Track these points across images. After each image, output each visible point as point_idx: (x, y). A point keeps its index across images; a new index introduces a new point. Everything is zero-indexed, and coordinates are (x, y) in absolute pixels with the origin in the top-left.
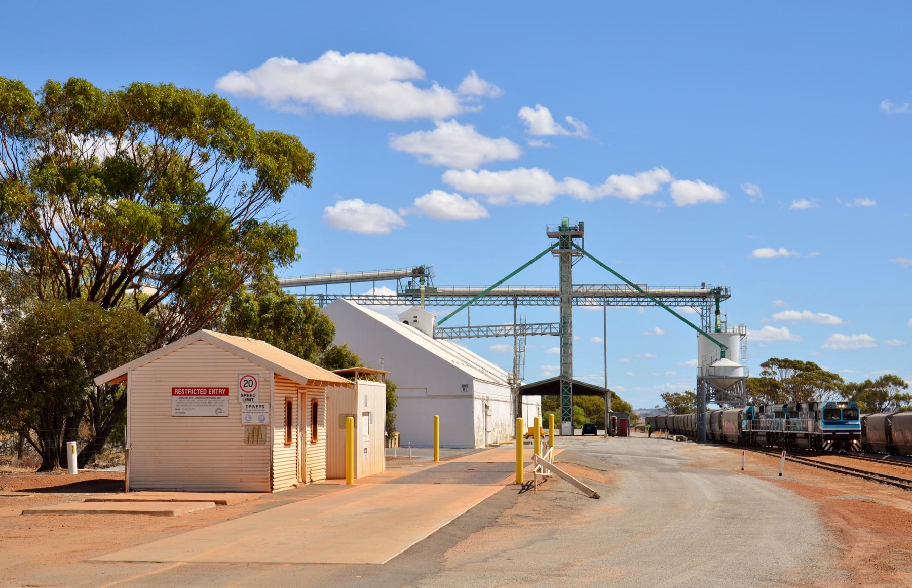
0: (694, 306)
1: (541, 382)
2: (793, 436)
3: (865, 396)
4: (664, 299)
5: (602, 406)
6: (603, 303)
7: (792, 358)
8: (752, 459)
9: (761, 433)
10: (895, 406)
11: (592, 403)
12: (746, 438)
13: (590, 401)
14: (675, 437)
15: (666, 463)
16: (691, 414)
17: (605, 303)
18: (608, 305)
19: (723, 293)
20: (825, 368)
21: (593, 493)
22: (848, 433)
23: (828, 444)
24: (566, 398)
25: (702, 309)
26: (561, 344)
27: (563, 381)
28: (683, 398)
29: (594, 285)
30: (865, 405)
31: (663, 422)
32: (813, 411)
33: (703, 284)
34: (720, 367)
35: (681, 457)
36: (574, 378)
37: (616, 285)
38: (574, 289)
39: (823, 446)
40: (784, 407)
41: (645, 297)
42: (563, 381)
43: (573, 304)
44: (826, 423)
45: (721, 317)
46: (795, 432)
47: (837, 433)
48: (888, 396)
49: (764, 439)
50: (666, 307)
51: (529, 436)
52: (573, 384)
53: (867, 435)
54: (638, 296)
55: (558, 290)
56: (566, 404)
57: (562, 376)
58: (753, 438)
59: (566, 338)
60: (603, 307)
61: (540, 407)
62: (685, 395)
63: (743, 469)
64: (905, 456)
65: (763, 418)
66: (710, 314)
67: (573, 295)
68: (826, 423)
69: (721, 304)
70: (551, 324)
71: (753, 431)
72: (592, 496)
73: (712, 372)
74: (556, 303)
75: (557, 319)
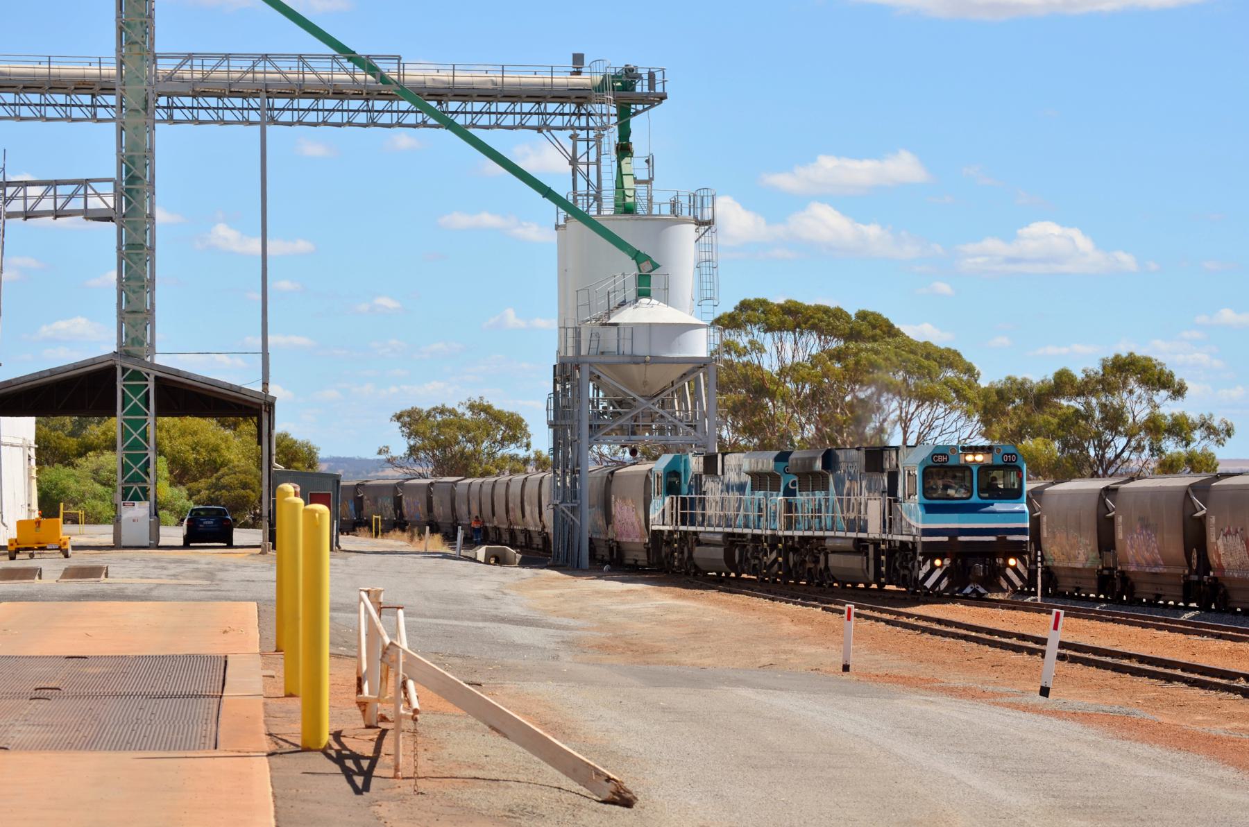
0: (549, 129)
1: (52, 372)
2: (812, 547)
3: (1055, 421)
4: (453, 106)
5: (917, 501)
6: (254, 116)
7: (809, 298)
8: (788, 627)
9: (708, 537)
10: (1147, 451)
11: (189, 439)
12: (665, 550)
13: (183, 434)
14: (481, 552)
15: (518, 640)
16: (504, 478)
17: (262, 116)
18: (274, 121)
19: (641, 87)
20: (917, 329)
21: (611, 786)
22: (993, 538)
23: (933, 568)
24: (136, 425)
25: (574, 137)
26: (119, 249)
27: (124, 370)
28: (463, 427)
29: (227, 57)
30: (1056, 445)
31: (388, 503)
32: (882, 471)
33: (578, 59)
34: (634, 327)
35: (553, 619)
36: (159, 360)
37: (300, 57)
38: (164, 67)
39: (921, 576)
40: (777, 459)
41: (390, 97)
42: (124, 370)
43: (157, 117)
44: (929, 509)
45: (635, 166)
47: (961, 539)
48: (1125, 422)
49: (719, 553)
50: (462, 132)
51: (17, 551)
52: (157, 378)
53: (1118, 545)
54: (367, 94)
55: (110, 70)
56: (135, 445)
57: (123, 353)
58: (682, 553)
59: (135, 230)
60: (258, 127)
61: (33, 453)
62: (468, 415)
63: (846, 668)
64: (1152, 604)
65: (713, 489)
66: (599, 153)
67: (161, 89)
68: (929, 509)
69: (635, 123)
70: (86, 183)
71: (682, 528)
72: (607, 795)
73: (610, 339)
74: (102, 113)
75: (107, 165)
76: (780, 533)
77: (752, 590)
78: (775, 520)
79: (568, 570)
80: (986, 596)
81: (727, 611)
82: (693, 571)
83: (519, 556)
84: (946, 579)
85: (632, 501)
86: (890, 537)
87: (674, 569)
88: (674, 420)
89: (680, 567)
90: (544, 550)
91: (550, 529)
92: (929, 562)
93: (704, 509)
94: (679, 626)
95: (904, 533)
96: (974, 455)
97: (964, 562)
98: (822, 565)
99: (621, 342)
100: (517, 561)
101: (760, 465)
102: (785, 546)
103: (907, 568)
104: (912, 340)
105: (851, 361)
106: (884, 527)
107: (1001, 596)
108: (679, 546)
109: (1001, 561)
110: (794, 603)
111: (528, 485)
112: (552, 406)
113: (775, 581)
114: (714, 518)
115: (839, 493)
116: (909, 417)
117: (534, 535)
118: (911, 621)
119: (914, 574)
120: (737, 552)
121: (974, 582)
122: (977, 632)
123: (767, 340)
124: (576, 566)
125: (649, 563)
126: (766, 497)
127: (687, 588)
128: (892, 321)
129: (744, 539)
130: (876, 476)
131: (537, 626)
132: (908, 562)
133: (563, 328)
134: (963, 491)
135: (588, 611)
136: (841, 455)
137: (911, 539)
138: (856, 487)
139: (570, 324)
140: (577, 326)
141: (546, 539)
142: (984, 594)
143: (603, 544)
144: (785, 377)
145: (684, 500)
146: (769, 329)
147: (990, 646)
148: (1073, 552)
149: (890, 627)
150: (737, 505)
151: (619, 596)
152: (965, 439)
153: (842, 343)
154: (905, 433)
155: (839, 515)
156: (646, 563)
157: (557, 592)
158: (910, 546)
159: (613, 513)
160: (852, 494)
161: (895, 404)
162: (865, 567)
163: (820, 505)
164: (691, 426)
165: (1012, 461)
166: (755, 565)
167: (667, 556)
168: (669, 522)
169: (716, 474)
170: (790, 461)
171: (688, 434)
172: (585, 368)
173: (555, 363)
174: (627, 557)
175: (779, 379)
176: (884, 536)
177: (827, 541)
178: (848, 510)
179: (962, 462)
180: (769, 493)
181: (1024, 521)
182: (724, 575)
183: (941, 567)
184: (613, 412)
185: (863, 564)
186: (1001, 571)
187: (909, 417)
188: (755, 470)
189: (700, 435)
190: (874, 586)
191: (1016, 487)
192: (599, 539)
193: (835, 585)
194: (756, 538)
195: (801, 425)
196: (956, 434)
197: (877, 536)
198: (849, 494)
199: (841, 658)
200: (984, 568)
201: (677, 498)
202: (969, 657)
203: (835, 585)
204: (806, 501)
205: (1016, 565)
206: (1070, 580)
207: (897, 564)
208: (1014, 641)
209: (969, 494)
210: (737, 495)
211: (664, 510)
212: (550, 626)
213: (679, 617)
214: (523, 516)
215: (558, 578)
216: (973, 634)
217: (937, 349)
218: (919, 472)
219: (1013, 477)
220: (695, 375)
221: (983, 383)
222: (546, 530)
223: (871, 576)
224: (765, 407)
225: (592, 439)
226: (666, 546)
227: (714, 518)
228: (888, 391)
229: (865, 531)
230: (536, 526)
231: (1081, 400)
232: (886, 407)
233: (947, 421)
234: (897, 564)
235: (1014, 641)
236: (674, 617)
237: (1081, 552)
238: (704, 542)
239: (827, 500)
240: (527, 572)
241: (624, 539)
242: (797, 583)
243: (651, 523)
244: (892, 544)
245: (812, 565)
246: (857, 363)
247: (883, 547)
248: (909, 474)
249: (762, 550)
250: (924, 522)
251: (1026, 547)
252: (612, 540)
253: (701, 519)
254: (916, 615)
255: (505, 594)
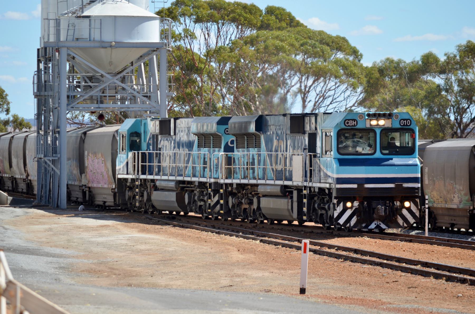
5: (333, 157)
8: (236, 256)
9: (164, 184)
12: (128, 194)
15: (25, 267)
22: (392, 186)
30: (424, 112)
32: (304, 133)
34: (102, 19)
35: (48, 249)
39: (336, 215)
40: (219, 123)
44: (342, 162)
46: (253, 182)
47: (367, 186)
49: (172, 197)
58: (142, 196)
63: (303, 291)
68: (342, 162)
76: (222, 181)
77: (199, 225)
78: (217, 171)
79: (50, 209)
80: (386, 231)
81: (184, 243)
82: (151, 210)
83: (10, 198)
84: (355, 217)
85: (102, 156)
86: (310, 184)
87: (136, 209)
88: (133, 92)
89: (140, 208)
90: (27, 193)
91: (34, 177)
92: (342, 204)
93: (159, 162)
94: (149, 255)
95: (322, 181)
96: (378, 120)
97: (369, 205)
98: (255, 206)
99: (92, 31)
100: (9, 202)
101: (205, 128)
102: (225, 191)
103: (324, 209)
104: (310, 29)
105: (262, 46)
106: (306, 176)
107: (394, 231)
108: (140, 190)
109: (398, 203)
110: (237, 236)
111: (14, 142)
112: (36, 82)
113: (216, 218)
114: (168, 169)
115: (269, 149)
116: (307, 89)
117: (19, 181)
118: (333, 251)
119: (330, 213)
120: (186, 196)
121: (377, 219)
122: (387, 260)
123: (198, 30)
124: (56, 206)
125: (115, 204)
126: (210, 153)
127: (148, 223)
128: (294, 14)
129: (192, 186)
130: (299, 137)
131: (37, 255)
132: (325, 204)
133: (46, 19)
134: (368, 148)
135: (74, 242)
136: (271, 120)
137: (327, 186)
138: (283, 146)
139: (52, 16)
140: (57, 18)
141: (29, 185)
142: (385, 229)
143: (77, 189)
144: (210, 58)
145: (144, 154)
146: (198, 20)
147: (402, 271)
148: (449, 196)
149: (318, 256)
150: (186, 159)
151: (96, 230)
152: (351, 107)
153: (255, 32)
154: (304, 101)
155: (269, 167)
156: (112, 204)
157: (47, 226)
158: (327, 191)
159: (86, 165)
160: (279, 151)
161: (296, 79)
162: (290, 208)
163: (253, 159)
164: (147, 97)
165: (407, 125)
166: (201, 206)
167: (129, 198)
168: (132, 172)
169: (170, 134)
170: (229, 124)
171: (143, 102)
172: (64, 52)
173: (39, 47)
174: (97, 199)
175: (207, 59)
176: (305, 184)
177: (259, 187)
178: (276, 163)
179: (368, 126)
180: (212, 149)
181: (417, 173)
182: (174, 213)
183: (351, 208)
184: (85, 86)
185: (288, 205)
186: (398, 211)
187: (307, 89)
188: (201, 132)
189: (154, 104)
190: (296, 223)
191: (410, 145)
192: (74, 185)
193: (265, 221)
194: (202, 185)
195: (222, 95)
196: (344, 103)
197: (300, 184)
198: (276, 151)
199: (299, 283)
200: (385, 209)
201: (138, 153)
202: (388, 280)
203: (265, 221)
204: (242, 156)
205: (410, 207)
206: (447, 218)
207: (316, 206)
208: (419, 267)
209: (373, 151)
210: (187, 151)
211: (127, 163)
212: (48, 255)
213: (147, 247)
214: (11, 166)
215: (43, 216)
216: (385, 261)
217: (329, 37)
218: (334, 134)
219: (407, 137)
220: (150, 57)
221: (367, 62)
222: (29, 178)
223: (295, 215)
224: (194, 82)
225: (69, 107)
226: (128, 191)
227: (168, 169)
228: (292, 69)
229: (290, 179)
230: (21, 174)
231: (443, 76)
232: (288, 81)
233: (336, 92)
234: (316, 206)
235: (419, 267)
236: (143, 247)
237: (456, 196)
238: (160, 188)
239: (259, 155)
240: (19, 211)
241: (95, 185)
242: (233, 220)
243: (117, 173)
244: (312, 190)
245: (247, 206)
246: (266, 48)
247: (305, 192)
248: (326, 135)
249: (206, 194)
250: (338, 173)
251: (418, 193)
252: (85, 185)
253: (157, 170)
254: (336, 246)
255: (6, 229)
